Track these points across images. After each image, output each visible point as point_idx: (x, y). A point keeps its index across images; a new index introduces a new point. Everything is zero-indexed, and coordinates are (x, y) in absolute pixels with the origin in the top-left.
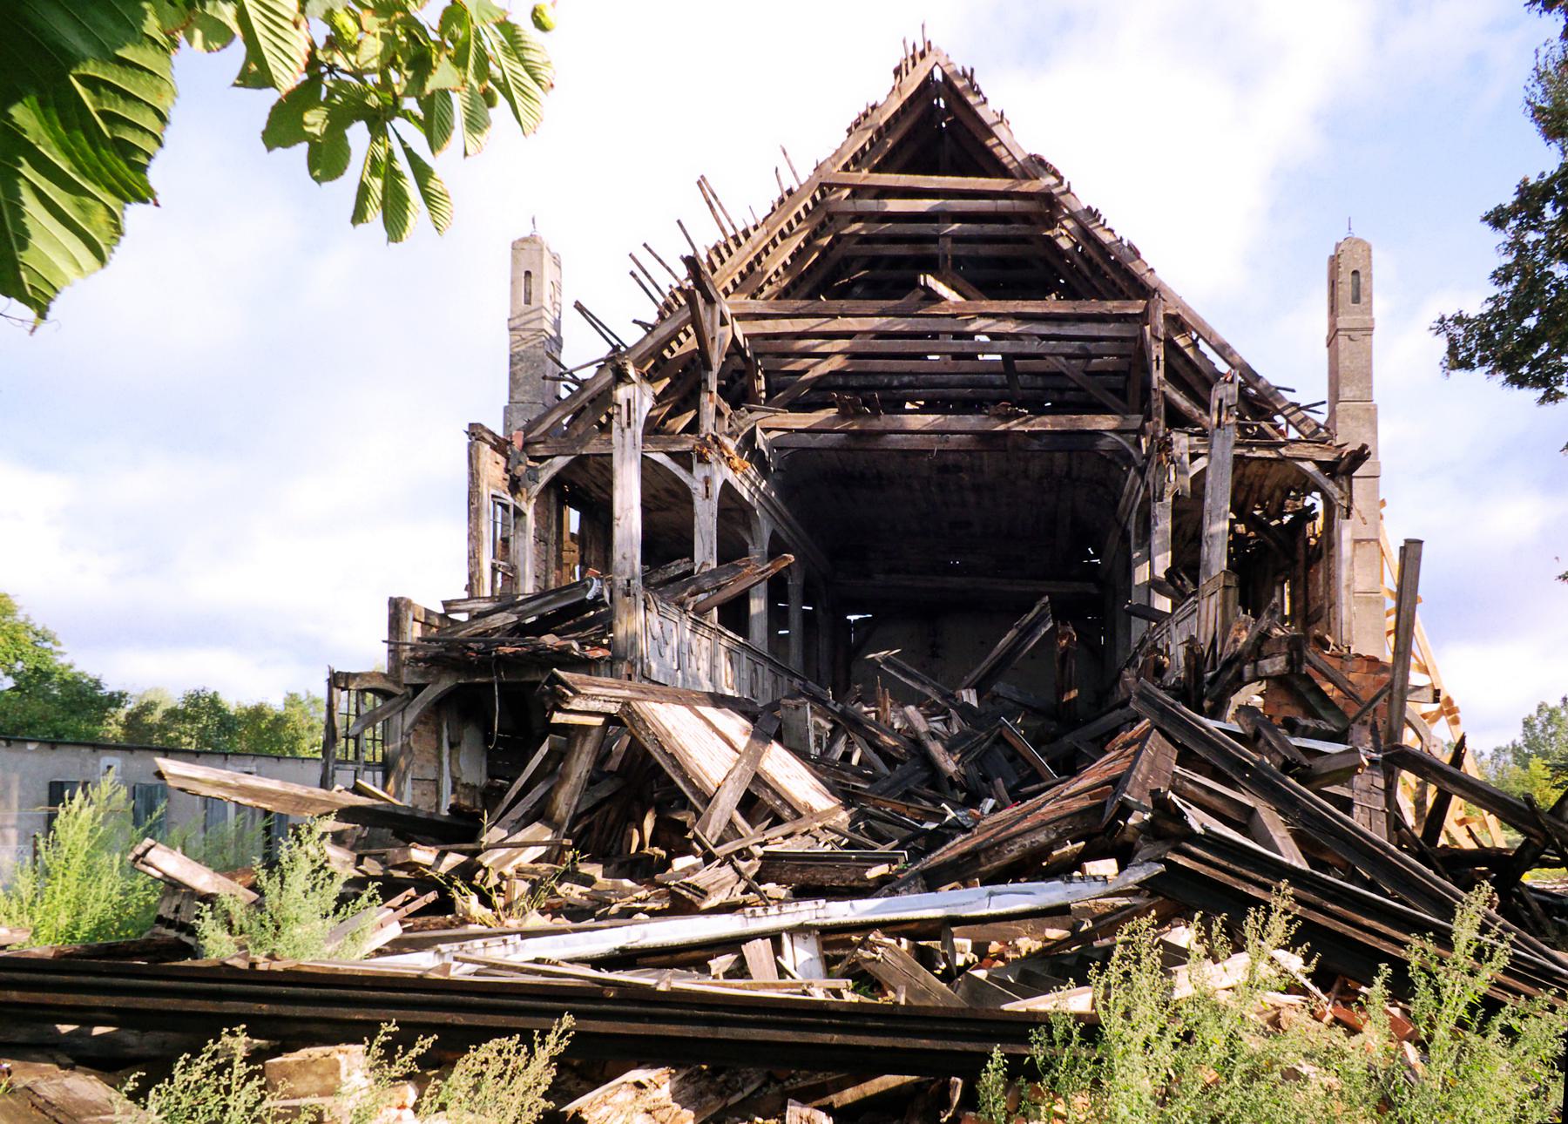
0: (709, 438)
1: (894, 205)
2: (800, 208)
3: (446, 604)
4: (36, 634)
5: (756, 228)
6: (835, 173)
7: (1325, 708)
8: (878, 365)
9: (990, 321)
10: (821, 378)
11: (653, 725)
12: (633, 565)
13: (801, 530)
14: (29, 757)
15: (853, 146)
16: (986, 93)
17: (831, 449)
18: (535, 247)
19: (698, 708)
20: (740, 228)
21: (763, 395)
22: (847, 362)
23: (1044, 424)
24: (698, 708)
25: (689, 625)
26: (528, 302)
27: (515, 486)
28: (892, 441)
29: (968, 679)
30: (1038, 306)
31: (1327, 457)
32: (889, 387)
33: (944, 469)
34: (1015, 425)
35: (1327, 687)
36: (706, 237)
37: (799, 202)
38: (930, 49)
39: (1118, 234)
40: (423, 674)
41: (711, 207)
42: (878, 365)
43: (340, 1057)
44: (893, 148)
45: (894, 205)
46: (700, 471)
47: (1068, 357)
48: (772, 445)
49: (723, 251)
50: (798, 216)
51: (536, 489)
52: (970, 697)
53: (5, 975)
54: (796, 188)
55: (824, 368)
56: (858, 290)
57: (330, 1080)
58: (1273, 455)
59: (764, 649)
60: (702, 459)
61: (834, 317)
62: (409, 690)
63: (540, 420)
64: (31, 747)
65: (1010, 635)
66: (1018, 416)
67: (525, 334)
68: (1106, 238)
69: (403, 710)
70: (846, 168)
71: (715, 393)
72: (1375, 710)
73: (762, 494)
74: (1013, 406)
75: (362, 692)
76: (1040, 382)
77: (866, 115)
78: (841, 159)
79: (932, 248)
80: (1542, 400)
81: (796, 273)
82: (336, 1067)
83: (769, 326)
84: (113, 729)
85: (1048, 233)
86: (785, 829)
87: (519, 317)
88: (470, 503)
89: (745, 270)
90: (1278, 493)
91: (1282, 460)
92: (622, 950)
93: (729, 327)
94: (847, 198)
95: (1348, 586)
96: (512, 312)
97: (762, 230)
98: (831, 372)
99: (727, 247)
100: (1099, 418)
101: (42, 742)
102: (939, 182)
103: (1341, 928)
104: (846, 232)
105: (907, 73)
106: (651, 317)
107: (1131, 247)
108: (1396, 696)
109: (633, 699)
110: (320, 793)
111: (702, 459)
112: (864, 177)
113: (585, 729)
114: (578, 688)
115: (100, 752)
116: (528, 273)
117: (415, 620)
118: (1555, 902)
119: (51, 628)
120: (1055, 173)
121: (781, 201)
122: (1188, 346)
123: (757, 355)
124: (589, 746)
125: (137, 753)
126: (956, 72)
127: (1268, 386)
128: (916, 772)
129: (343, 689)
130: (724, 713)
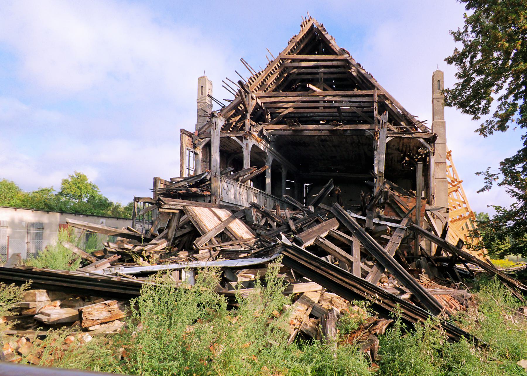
1: (304, 64)
2: (276, 65)
3: (171, 179)
6: (285, 55)
7: (401, 213)
8: (302, 110)
9: (331, 97)
10: (286, 114)
11: (191, 213)
13: (285, 159)
15: (289, 48)
16: (327, 31)
17: (288, 135)
18: (204, 79)
19: (213, 209)
20: (257, 73)
21: (270, 120)
22: (294, 110)
23: (347, 127)
24: (213, 209)
25: (238, 186)
26: (202, 95)
27: (195, 147)
28: (306, 133)
29: (312, 203)
30: (343, 93)
31: (426, 137)
32: (307, 117)
33: (322, 141)
34: (338, 128)
35: (402, 207)
36: (246, 76)
38: (311, 19)
39: (366, 71)
42: (302, 110)
43: (37, 292)
44: (303, 47)
45: (304, 64)
46: (245, 142)
47: (357, 107)
48: (270, 134)
49: (253, 79)
50: (275, 67)
51: (201, 147)
52: (312, 208)
54: (273, 60)
55: (287, 112)
56: (299, 89)
57: (34, 298)
58: (410, 136)
59: (270, 193)
60: (246, 139)
61: (286, 97)
63: (202, 128)
64: (81, 216)
65: (323, 190)
66: (340, 125)
67: (201, 104)
68: (363, 72)
70: (289, 53)
71: (250, 120)
72: (412, 214)
73: (268, 148)
74: (337, 122)
75: (145, 203)
76: (350, 115)
77: (293, 39)
78: (286, 51)
79: (318, 76)
80: (473, 119)
81: (277, 84)
82: (35, 295)
83: (268, 100)
85: (349, 71)
86: (231, 243)
87: (200, 99)
88: (181, 151)
90: (415, 148)
91: (413, 138)
92: (142, 272)
93: (255, 101)
94: (290, 62)
95: (433, 176)
96: (198, 97)
97: (264, 73)
98: (289, 113)
99: (254, 78)
100: (363, 125)
101: (84, 215)
102: (314, 57)
103: (324, 274)
104: (291, 72)
105: (305, 26)
106: (233, 98)
107: (370, 74)
108: (417, 210)
109: (187, 206)
111: (246, 139)
112: (295, 56)
113: (174, 214)
114: (166, 202)
115: (100, 218)
116: (202, 87)
118: (465, 273)
119: (97, 185)
120: (348, 53)
121: (269, 64)
122: (389, 104)
123: (267, 108)
124: (176, 218)
125: (109, 219)
126: (319, 25)
127: (411, 116)
128: (284, 229)
129: (138, 202)
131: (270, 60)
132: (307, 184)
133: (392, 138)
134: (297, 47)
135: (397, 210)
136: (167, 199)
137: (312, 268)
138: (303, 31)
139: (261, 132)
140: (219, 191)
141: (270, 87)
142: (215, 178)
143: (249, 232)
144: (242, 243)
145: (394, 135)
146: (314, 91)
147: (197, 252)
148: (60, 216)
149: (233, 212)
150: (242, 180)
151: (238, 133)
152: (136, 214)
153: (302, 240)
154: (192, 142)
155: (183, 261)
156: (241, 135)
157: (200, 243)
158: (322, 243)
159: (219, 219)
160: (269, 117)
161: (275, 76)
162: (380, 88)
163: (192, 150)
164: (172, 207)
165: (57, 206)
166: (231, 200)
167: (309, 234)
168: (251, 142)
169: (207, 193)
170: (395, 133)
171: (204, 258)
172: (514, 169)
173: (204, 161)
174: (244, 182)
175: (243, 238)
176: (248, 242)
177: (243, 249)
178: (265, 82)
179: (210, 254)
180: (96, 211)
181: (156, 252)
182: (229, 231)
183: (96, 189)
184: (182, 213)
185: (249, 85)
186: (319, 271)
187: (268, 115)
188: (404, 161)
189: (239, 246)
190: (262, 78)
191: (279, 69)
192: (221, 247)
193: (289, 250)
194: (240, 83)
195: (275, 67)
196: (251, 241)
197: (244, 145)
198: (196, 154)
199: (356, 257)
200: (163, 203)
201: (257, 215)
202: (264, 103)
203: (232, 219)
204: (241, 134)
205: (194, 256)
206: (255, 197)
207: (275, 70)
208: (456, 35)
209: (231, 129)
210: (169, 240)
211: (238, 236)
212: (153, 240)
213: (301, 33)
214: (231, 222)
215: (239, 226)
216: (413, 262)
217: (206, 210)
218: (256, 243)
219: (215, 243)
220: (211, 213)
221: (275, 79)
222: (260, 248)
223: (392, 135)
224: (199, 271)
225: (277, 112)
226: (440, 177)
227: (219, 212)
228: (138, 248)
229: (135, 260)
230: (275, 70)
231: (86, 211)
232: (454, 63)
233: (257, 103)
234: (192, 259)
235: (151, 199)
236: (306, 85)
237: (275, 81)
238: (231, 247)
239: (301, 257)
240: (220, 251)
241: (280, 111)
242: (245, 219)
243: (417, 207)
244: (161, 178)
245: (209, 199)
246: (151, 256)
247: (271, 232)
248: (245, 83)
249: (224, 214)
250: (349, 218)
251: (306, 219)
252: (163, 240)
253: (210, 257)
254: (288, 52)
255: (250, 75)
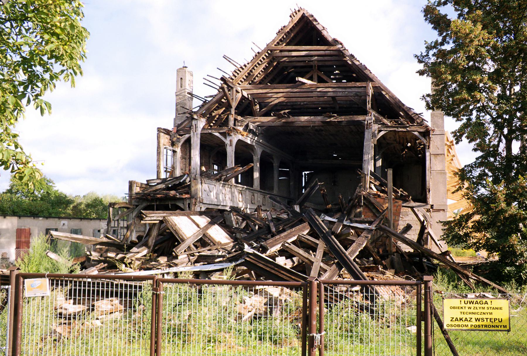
0: (231, 128)
1: (294, 54)
3: (147, 181)
4: (48, 181)
5: (248, 64)
8: (294, 100)
11: (171, 222)
12: (196, 171)
14: (40, 222)
15: (278, 38)
19: (191, 217)
21: (258, 110)
23: (342, 119)
24: (191, 217)
26: (181, 87)
27: (173, 144)
31: (422, 130)
33: (316, 130)
34: (332, 119)
36: (229, 70)
37: (261, 56)
39: (361, 62)
40: (138, 202)
41: (230, 62)
44: (293, 38)
46: (229, 138)
49: (238, 72)
51: (180, 144)
52: (297, 208)
53: (423, 354)
55: (277, 101)
58: (405, 130)
62: (135, 207)
64: (41, 219)
68: (357, 63)
69: (132, 212)
77: (282, 29)
79: (311, 63)
84: (69, 211)
88: (158, 151)
89: (247, 75)
91: (408, 131)
96: (177, 90)
99: (239, 70)
100: (359, 117)
102: (305, 48)
103: (277, 273)
105: (294, 16)
107: (364, 66)
109: (167, 216)
110: (93, 238)
112: (283, 46)
113: (154, 224)
115: (61, 220)
116: (181, 78)
117: (137, 186)
119: (52, 179)
120: (341, 44)
121: (256, 56)
122: (386, 94)
124: (156, 227)
125: (72, 220)
130: (203, 217)
131: (257, 52)
132: (306, 172)
133: (386, 132)
134: (286, 36)
135: (374, 211)
136: (148, 212)
137: (268, 269)
138: (292, 21)
139: (247, 126)
140: (200, 194)
141: (258, 77)
142: (195, 181)
143: (228, 236)
144: (220, 247)
145: (388, 129)
146: (304, 84)
147: (176, 257)
148: (18, 220)
149: (212, 217)
150: (224, 179)
151: (221, 129)
152: (111, 219)
153: (267, 246)
154: (170, 140)
155: (164, 266)
156: (224, 131)
157: (181, 251)
158: (287, 247)
159: (198, 226)
160: (258, 107)
161: (263, 66)
162: (375, 79)
163: (171, 148)
164: (152, 218)
165: (10, 208)
166: (212, 201)
167: (276, 240)
168: (235, 138)
169: (187, 196)
170: (388, 127)
171: (183, 263)
172: (471, 175)
173: (183, 158)
174: (227, 181)
175: (221, 243)
176: (226, 246)
177: (220, 254)
178: (252, 72)
179: (189, 259)
180: (54, 211)
181: (137, 259)
182: (207, 237)
183: (51, 184)
184: (161, 222)
185: (233, 78)
186: (273, 271)
187: (256, 105)
188: (404, 152)
189: (217, 250)
190: (248, 70)
191: (267, 59)
192: (199, 252)
193: (251, 257)
194: (222, 79)
195: (263, 58)
196: (229, 245)
197: (227, 141)
198: (174, 152)
199: (318, 258)
200: (144, 216)
201: (237, 219)
202: (250, 94)
203: (210, 225)
204: (225, 130)
205: (174, 261)
206: (240, 195)
207: (262, 60)
208: (419, 58)
209: (214, 122)
210: (148, 247)
211: (216, 242)
212: (134, 248)
213: (291, 24)
214: (209, 228)
215: (217, 231)
216: (388, 258)
217: (185, 218)
218: (234, 247)
219: (193, 249)
220: (190, 221)
221: (264, 69)
222: (238, 251)
223: (386, 129)
224: (179, 275)
225: (267, 101)
226: (439, 169)
227: (197, 218)
228: (120, 256)
229: (118, 267)
230: (262, 60)
231: (43, 211)
232: (426, 75)
233: (243, 96)
234: (172, 264)
235: (126, 203)
236: (296, 78)
237: (263, 70)
238: (209, 252)
239: (260, 261)
240: (198, 256)
241: (269, 100)
242: (225, 223)
243: (389, 208)
244: (137, 181)
245: (188, 201)
246: (133, 262)
247: (252, 235)
248: (227, 76)
249: (203, 221)
250: (319, 223)
251: (290, 220)
252: (144, 247)
253: (189, 262)
254: (276, 42)
255: (234, 68)
